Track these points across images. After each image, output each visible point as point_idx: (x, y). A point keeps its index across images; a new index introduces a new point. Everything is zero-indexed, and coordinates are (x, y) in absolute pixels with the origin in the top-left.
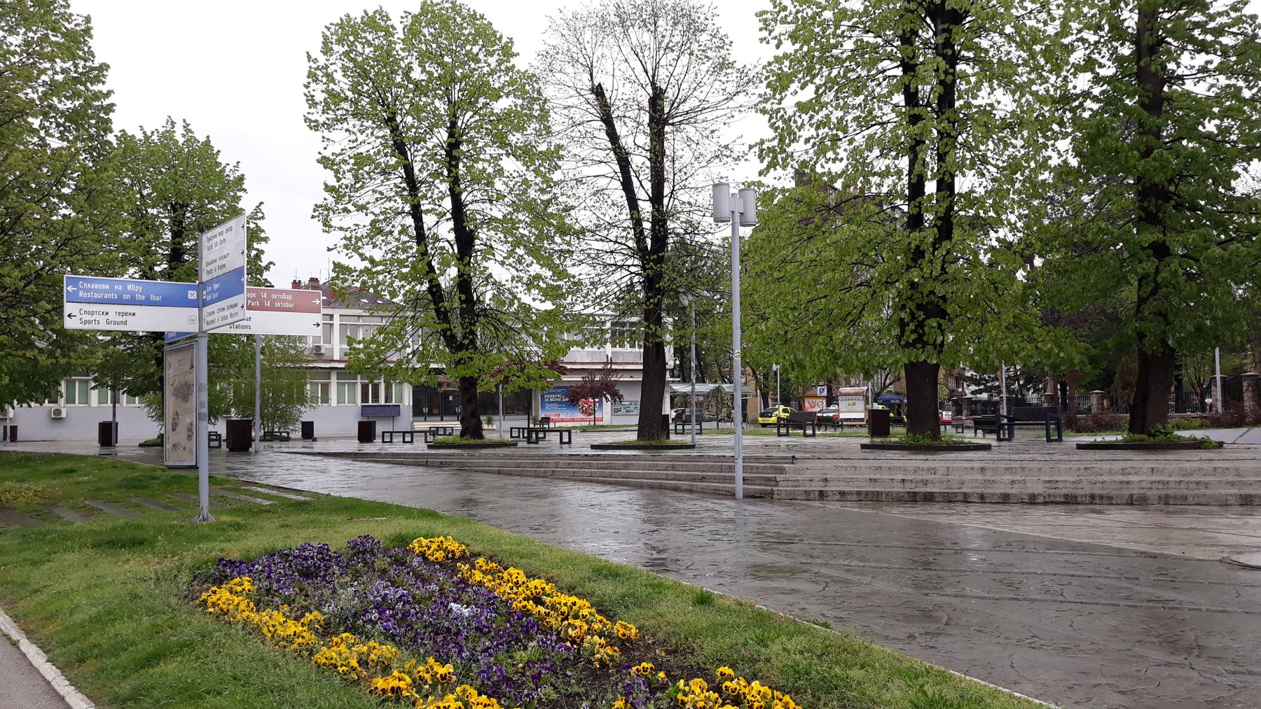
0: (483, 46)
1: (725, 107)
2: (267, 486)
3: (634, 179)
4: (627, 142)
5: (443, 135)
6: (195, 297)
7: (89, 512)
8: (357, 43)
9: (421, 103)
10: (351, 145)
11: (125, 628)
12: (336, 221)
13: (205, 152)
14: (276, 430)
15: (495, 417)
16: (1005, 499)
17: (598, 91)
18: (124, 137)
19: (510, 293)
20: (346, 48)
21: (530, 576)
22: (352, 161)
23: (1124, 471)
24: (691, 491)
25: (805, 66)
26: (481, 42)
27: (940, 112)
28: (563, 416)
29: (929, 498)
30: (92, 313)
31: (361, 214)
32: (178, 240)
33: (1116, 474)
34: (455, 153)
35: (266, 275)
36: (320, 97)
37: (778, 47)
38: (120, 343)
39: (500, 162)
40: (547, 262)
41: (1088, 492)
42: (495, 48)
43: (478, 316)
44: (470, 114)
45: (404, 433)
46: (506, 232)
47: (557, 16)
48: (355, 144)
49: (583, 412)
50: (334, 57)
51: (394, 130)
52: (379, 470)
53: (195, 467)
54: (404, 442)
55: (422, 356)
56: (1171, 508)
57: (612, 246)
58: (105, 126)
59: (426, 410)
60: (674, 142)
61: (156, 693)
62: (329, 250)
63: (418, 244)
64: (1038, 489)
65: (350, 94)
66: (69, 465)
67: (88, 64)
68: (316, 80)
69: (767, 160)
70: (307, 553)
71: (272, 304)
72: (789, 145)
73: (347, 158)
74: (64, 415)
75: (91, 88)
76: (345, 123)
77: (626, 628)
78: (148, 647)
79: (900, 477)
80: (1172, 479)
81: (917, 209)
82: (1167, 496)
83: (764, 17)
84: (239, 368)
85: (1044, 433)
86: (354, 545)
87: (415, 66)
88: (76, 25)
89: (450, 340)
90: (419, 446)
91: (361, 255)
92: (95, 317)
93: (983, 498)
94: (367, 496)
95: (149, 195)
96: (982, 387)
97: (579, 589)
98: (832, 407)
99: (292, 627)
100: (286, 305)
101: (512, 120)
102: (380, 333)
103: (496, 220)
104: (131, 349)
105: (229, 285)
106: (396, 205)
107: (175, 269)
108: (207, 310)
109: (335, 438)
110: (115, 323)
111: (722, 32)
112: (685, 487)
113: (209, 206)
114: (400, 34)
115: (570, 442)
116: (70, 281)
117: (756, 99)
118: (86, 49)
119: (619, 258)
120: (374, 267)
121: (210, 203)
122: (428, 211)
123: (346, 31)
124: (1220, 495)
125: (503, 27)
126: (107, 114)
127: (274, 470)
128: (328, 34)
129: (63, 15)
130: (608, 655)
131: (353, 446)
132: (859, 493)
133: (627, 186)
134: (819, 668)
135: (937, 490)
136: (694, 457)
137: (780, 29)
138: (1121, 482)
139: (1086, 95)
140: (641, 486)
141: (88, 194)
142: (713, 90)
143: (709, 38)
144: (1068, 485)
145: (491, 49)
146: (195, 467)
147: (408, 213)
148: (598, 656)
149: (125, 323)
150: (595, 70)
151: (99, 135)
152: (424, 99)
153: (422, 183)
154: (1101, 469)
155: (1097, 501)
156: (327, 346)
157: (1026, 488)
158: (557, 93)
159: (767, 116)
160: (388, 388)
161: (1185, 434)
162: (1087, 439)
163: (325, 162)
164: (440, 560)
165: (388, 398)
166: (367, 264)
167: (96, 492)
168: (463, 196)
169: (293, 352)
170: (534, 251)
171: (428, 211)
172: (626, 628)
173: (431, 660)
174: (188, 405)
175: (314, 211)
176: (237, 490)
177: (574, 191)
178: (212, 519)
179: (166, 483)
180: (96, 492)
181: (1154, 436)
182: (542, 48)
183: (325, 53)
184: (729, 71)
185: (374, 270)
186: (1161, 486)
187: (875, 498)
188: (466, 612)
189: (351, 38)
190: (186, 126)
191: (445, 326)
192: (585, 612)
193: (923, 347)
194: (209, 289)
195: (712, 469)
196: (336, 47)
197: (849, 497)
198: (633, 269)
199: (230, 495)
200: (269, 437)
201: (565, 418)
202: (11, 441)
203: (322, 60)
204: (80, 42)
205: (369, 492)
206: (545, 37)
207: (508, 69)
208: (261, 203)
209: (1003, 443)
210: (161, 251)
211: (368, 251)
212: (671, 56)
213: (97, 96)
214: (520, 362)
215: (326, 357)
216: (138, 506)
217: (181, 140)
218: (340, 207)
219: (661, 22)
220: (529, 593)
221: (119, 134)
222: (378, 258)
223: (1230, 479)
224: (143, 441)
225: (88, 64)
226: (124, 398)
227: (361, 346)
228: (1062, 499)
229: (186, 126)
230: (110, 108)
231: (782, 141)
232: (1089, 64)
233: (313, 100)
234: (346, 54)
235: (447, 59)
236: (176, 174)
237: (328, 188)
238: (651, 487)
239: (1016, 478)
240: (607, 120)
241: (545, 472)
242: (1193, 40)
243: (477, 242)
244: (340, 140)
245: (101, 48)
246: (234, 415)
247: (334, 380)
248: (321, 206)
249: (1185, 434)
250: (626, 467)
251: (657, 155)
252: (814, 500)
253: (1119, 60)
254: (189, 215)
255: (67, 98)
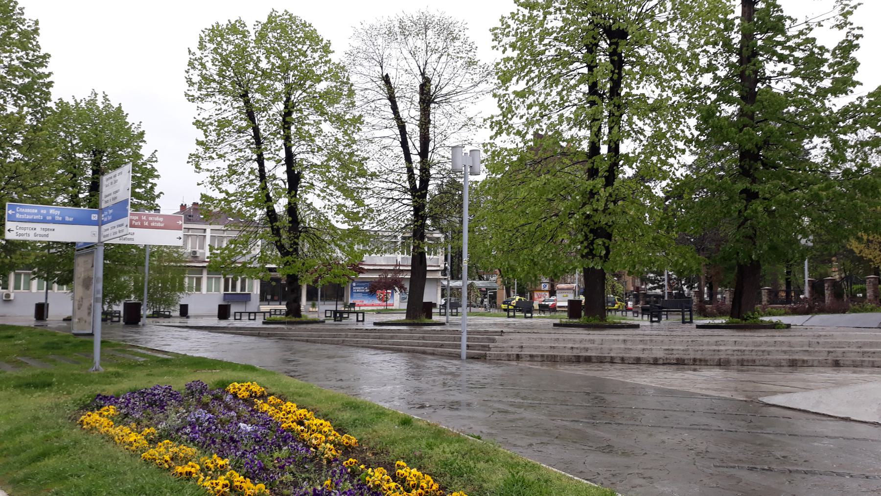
0: (310, 45)
1: (472, 91)
2: (145, 348)
3: (409, 140)
4: (404, 114)
5: (281, 106)
6: (96, 218)
7: (17, 364)
8: (223, 43)
9: (265, 85)
10: (217, 112)
11: (26, 438)
12: (204, 165)
13: (118, 114)
14: (162, 310)
15: (317, 303)
16: (638, 361)
17: (386, 79)
18: (61, 103)
19: (324, 217)
20: (215, 46)
21: (299, 407)
22: (216, 124)
23: (717, 343)
24: (433, 354)
25: (521, 68)
26: (308, 43)
27: (610, 98)
28: (366, 302)
29: (588, 360)
30: (25, 229)
31: (221, 161)
32: (96, 176)
33: (712, 345)
34: (287, 119)
35: (157, 201)
36: (196, 79)
37: (504, 52)
38: (53, 248)
39: (320, 126)
40: (348, 193)
41: (692, 357)
42: (318, 47)
43: (301, 232)
44: (300, 92)
45: (250, 313)
46: (322, 174)
47: (359, 27)
48: (220, 112)
49: (380, 300)
50: (207, 51)
51: (247, 102)
52: (225, 339)
53: (92, 335)
54: (250, 319)
55: (263, 259)
56: (745, 368)
57: (390, 185)
58: (47, 97)
59: (269, 297)
60: (437, 115)
61: (39, 477)
62: (198, 184)
63: (261, 181)
64: (659, 354)
65: (217, 78)
66: (10, 333)
67: (36, 54)
68: (194, 68)
69: (496, 129)
70: (156, 392)
71: (149, 224)
72: (511, 119)
73: (213, 122)
74: (12, 298)
75: (38, 70)
76: (214, 97)
77: (349, 439)
78: (41, 449)
79: (570, 345)
80: (747, 349)
81: (592, 165)
82: (743, 360)
83: (496, 31)
84: (136, 266)
85: (681, 317)
86: (189, 387)
87: (263, 58)
88: (28, 26)
89: (281, 248)
90: (258, 323)
91: (219, 189)
92: (26, 231)
93: (623, 360)
94: (227, 358)
95: (77, 144)
96: (656, 285)
97: (330, 416)
98: (552, 298)
99: (133, 437)
100: (159, 225)
101: (331, 97)
102: (231, 244)
103: (316, 165)
104: (60, 251)
105: (119, 211)
106: (247, 155)
107: (94, 196)
108: (104, 227)
109: (202, 316)
110: (41, 236)
111: (470, 41)
112: (430, 351)
113: (120, 152)
114: (253, 37)
115: (363, 321)
116: (10, 207)
117: (492, 86)
118: (34, 43)
119: (396, 194)
120: (229, 197)
121: (120, 150)
122: (269, 159)
123: (216, 33)
124: (777, 359)
125: (324, 33)
126: (47, 88)
127: (152, 337)
128: (203, 35)
129: (19, 20)
130: (332, 455)
131: (215, 322)
132: (542, 356)
133: (404, 144)
134: (460, 462)
135: (594, 354)
136: (438, 331)
137: (506, 40)
138: (714, 351)
139: (707, 89)
140: (400, 351)
141: (29, 147)
142: (464, 80)
143: (461, 44)
144: (679, 352)
145: (316, 47)
146: (92, 335)
147: (255, 160)
148: (326, 456)
149: (47, 236)
150: (384, 65)
151: (41, 103)
152: (268, 82)
153: (265, 138)
154: (702, 342)
155: (697, 363)
156: (201, 251)
157: (653, 354)
158: (358, 80)
159: (497, 99)
160: (243, 281)
161: (766, 319)
162: (707, 321)
163: (198, 124)
164: (245, 397)
165: (243, 288)
166: (223, 195)
167: (26, 352)
168: (293, 149)
169: (176, 255)
170: (342, 189)
171: (269, 159)
172: (349, 439)
173: (215, 456)
174: (89, 292)
175: (189, 158)
176: (123, 351)
177: (366, 148)
178: (102, 370)
179: (76, 346)
180: (26, 352)
181: (746, 320)
182: (348, 49)
183: (200, 49)
184: (475, 67)
185: (230, 199)
186: (739, 353)
187: (553, 360)
188: (249, 428)
189: (219, 39)
190: (105, 97)
191: (277, 238)
192: (326, 429)
193: (593, 258)
194: (106, 213)
195: (448, 339)
196: (208, 45)
197: (536, 359)
198: (405, 202)
199: (118, 354)
200: (157, 315)
201: (366, 303)
202: (460, 341)
203: (198, 54)
204: (31, 39)
205: (214, 353)
206: (351, 41)
207: (326, 62)
208: (156, 151)
209: (654, 324)
210: (84, 183)
211: (226, 186)
212: (435, 56)
213: (41, 76)
214: (330, 265)
215: (200, 259)
216: (54, 361)
217: (101, 106)
218: (208, 155)
219: (429, 32)
220: (295, 418)
221: (58, 102)
222: (231, 191)
223: (785, 348)
224: (65, 317)
225: (36, 54)
226: (56, 286)
227: (219, 252)
228: (675, 362)
229: (105, 97)
230: (50, 85)
231: (504, 115)
232: (711, 68)
233: (191, 81)
234: (215, 49)
235: (285, 54)
236: (96, 129)
237: (200, 143)
238: (408, 351)
239: (645, 347)
240: (392, 99)
241: (338, 341)
242: (775, 53)
243: (303, 180)
244: (209, 109)
245: (45, 42)
246: (133, 299)
247: (205, 275)
248: (194, 155)
249: (766, 319)
250: (392, 337)
251: (425, 123)
252: (513, 360)
253: (731, 65)
254: (105, 158)
255: (20, 77)
